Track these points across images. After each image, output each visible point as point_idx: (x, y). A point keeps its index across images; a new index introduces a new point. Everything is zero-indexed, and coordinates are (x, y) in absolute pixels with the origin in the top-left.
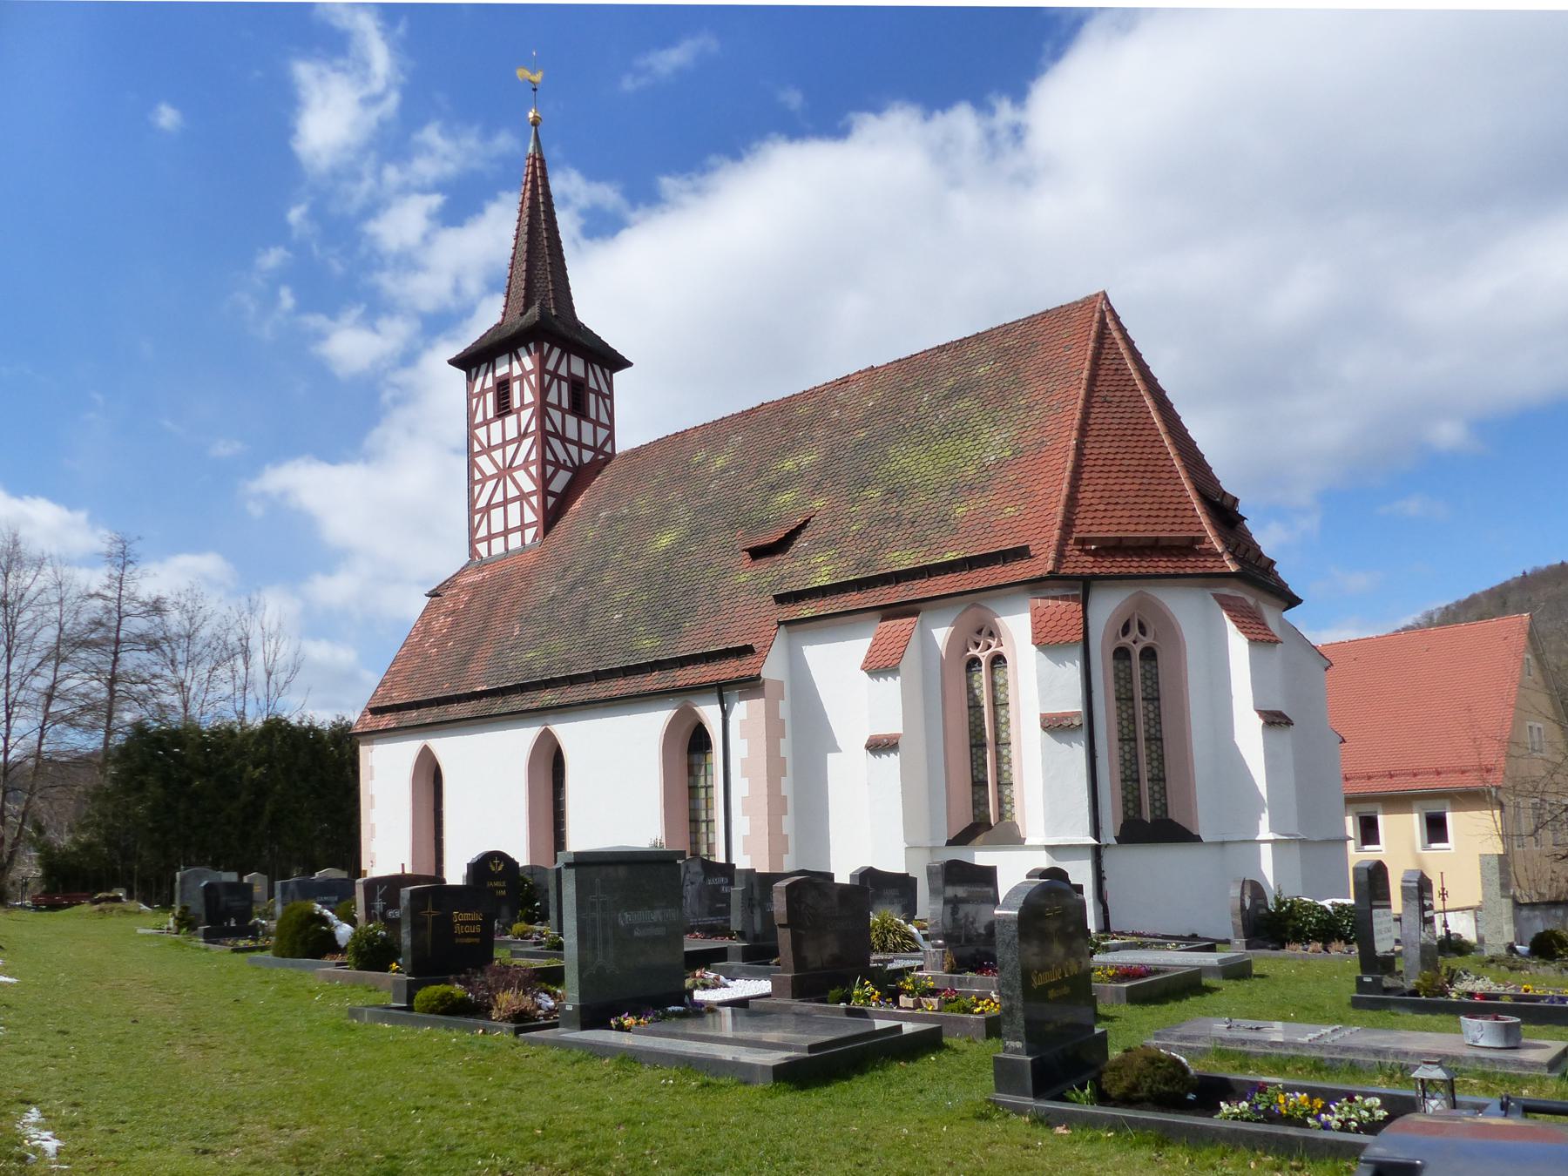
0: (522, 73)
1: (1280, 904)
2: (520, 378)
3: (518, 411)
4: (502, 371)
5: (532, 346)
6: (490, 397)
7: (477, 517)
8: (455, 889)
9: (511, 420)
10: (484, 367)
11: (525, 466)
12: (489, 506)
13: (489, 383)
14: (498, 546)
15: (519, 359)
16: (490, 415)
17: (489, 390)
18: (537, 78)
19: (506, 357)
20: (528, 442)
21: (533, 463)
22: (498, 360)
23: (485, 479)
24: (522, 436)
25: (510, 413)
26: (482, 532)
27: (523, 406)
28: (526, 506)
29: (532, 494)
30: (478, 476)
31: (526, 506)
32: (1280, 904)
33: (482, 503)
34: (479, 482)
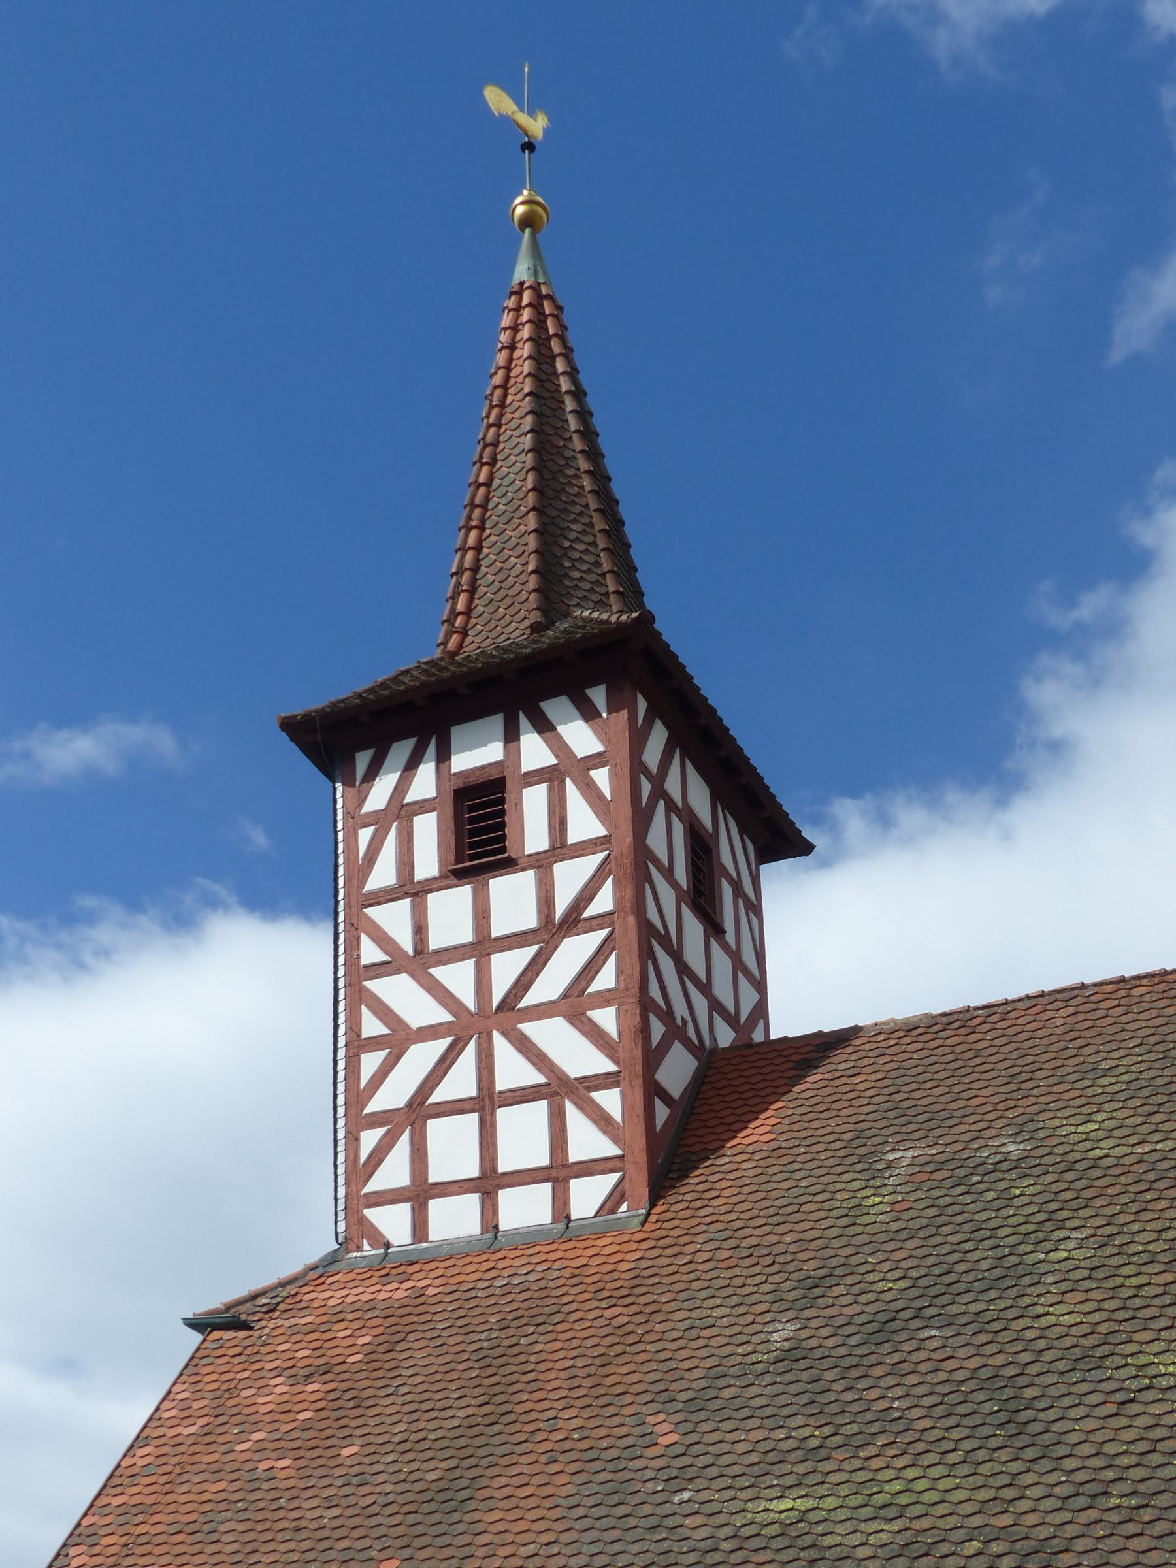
0: (497, 100)
1: (500, 114)
2: (552, 777)
3: (543, 864)
4: (477, 753)
5: (598, 695)
6: (426, 828)
7: (369, 1139)
8: (548, 114)
9: (513, 900)
10: (401, 751)
11: (574, 1004)
12: (419, 1111)
13: (425, 783)
14: (454, 1219)
15: (544, 726)
16: (427, 864)
17: (423, 807)
18: (537, 125)
19: (496, 722)
20: (575, 951)
21: (604, 999)
22: (458, 733)
23: (400, 1037)
24: (552, 930)
25: (509, 865)
26: (394, 1172)
27: (560, 849)
28: (572, 792)
29: (595, 761)
30: (372, 1026)
31: (572, 792)
32: (500, 114)
33: (394, 1094)
34: (375, 1043)
